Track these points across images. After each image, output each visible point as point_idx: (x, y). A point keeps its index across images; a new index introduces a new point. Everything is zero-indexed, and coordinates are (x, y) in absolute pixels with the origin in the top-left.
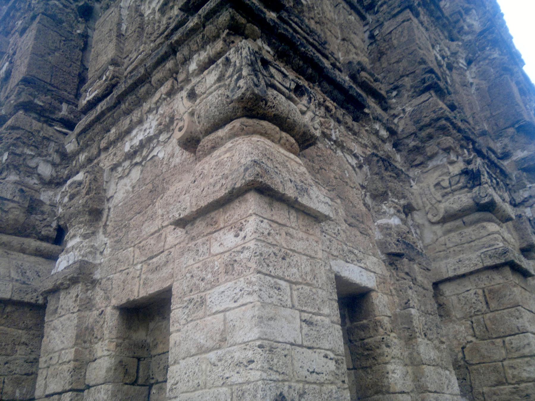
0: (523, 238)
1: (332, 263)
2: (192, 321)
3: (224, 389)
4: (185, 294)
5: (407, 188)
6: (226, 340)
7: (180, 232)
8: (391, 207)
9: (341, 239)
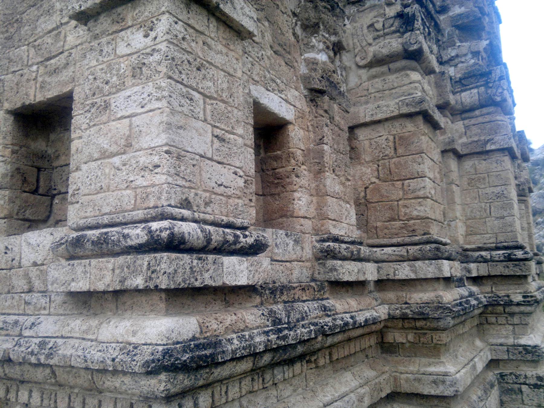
0: (440, 95)
1: (252, 87)
2: (94, 125)
3: (128, 192)
4: (87, 97)
5: (340, 24)
6: (131, 146)
7: (82, 30)
8: (320, 41)
9: (264, 65)
